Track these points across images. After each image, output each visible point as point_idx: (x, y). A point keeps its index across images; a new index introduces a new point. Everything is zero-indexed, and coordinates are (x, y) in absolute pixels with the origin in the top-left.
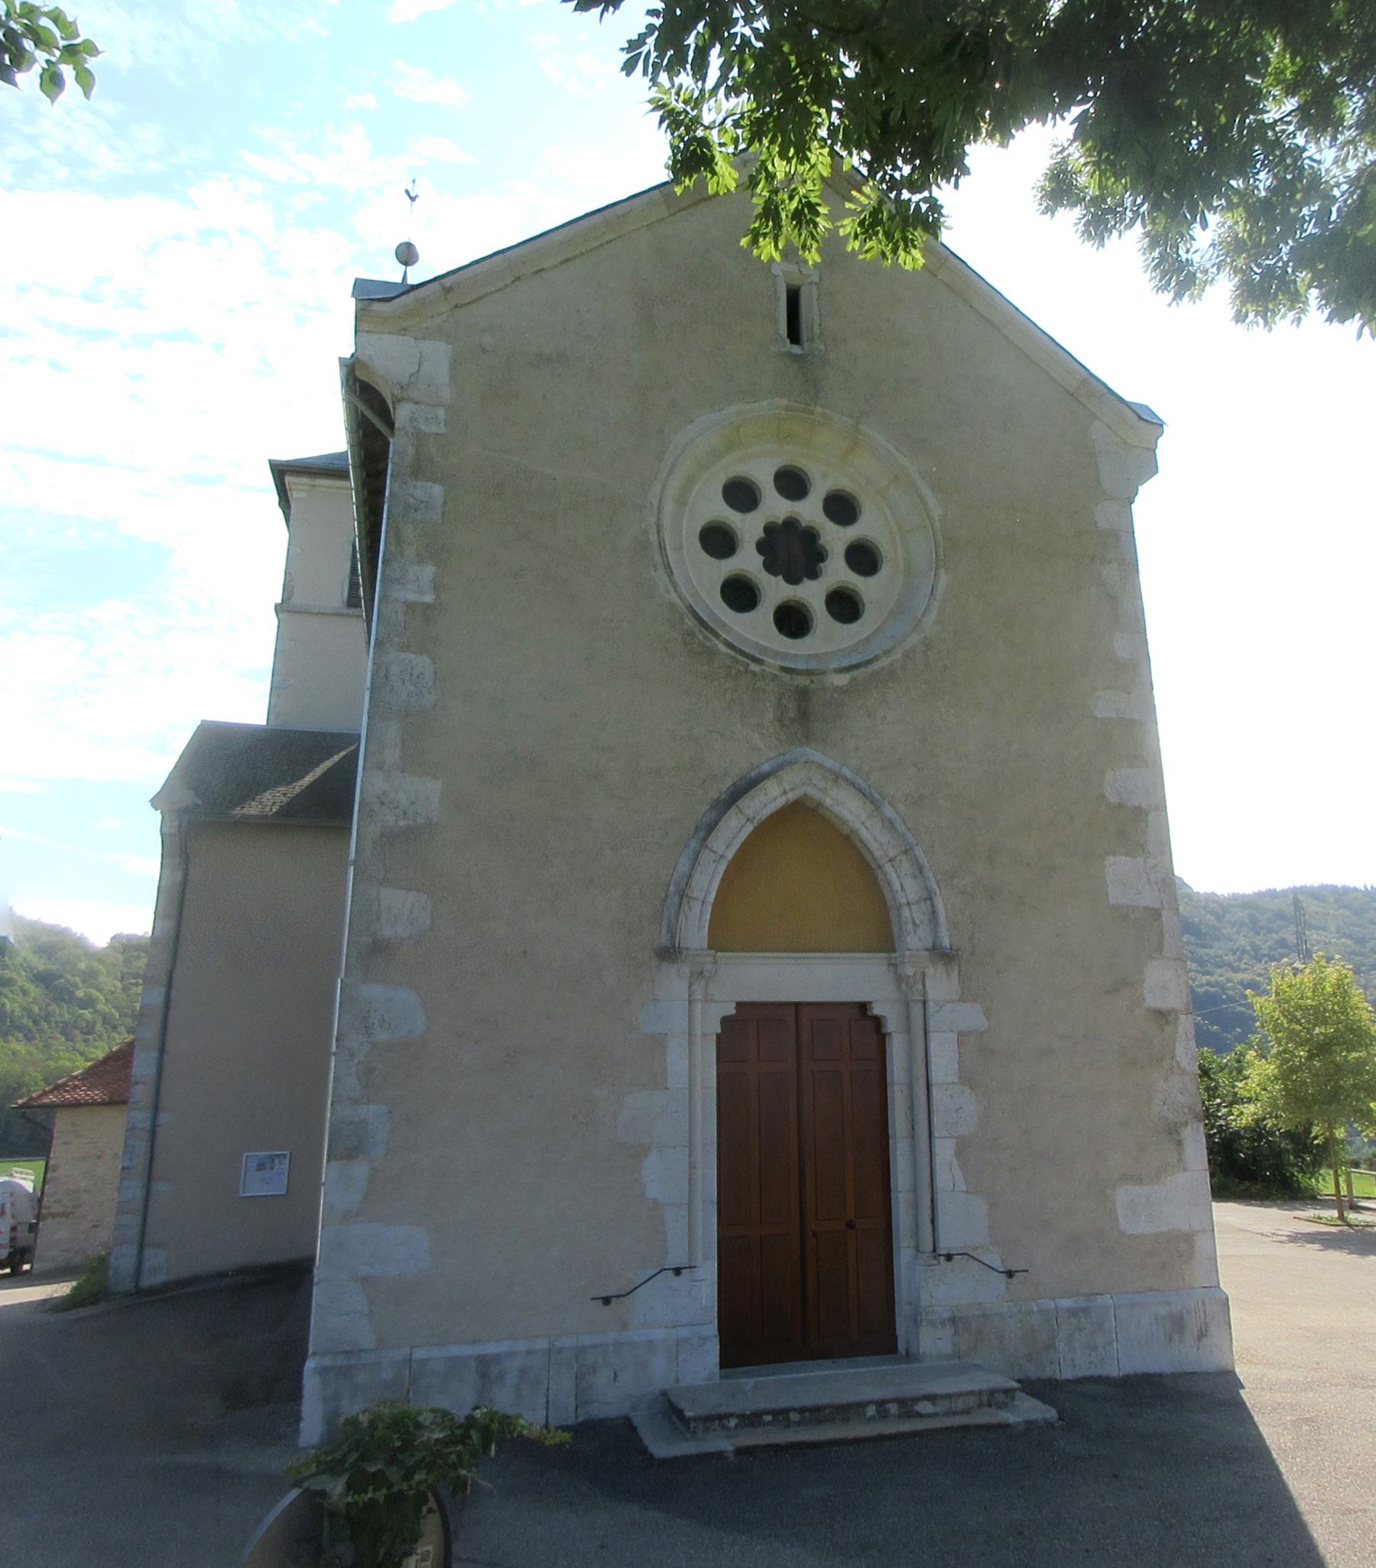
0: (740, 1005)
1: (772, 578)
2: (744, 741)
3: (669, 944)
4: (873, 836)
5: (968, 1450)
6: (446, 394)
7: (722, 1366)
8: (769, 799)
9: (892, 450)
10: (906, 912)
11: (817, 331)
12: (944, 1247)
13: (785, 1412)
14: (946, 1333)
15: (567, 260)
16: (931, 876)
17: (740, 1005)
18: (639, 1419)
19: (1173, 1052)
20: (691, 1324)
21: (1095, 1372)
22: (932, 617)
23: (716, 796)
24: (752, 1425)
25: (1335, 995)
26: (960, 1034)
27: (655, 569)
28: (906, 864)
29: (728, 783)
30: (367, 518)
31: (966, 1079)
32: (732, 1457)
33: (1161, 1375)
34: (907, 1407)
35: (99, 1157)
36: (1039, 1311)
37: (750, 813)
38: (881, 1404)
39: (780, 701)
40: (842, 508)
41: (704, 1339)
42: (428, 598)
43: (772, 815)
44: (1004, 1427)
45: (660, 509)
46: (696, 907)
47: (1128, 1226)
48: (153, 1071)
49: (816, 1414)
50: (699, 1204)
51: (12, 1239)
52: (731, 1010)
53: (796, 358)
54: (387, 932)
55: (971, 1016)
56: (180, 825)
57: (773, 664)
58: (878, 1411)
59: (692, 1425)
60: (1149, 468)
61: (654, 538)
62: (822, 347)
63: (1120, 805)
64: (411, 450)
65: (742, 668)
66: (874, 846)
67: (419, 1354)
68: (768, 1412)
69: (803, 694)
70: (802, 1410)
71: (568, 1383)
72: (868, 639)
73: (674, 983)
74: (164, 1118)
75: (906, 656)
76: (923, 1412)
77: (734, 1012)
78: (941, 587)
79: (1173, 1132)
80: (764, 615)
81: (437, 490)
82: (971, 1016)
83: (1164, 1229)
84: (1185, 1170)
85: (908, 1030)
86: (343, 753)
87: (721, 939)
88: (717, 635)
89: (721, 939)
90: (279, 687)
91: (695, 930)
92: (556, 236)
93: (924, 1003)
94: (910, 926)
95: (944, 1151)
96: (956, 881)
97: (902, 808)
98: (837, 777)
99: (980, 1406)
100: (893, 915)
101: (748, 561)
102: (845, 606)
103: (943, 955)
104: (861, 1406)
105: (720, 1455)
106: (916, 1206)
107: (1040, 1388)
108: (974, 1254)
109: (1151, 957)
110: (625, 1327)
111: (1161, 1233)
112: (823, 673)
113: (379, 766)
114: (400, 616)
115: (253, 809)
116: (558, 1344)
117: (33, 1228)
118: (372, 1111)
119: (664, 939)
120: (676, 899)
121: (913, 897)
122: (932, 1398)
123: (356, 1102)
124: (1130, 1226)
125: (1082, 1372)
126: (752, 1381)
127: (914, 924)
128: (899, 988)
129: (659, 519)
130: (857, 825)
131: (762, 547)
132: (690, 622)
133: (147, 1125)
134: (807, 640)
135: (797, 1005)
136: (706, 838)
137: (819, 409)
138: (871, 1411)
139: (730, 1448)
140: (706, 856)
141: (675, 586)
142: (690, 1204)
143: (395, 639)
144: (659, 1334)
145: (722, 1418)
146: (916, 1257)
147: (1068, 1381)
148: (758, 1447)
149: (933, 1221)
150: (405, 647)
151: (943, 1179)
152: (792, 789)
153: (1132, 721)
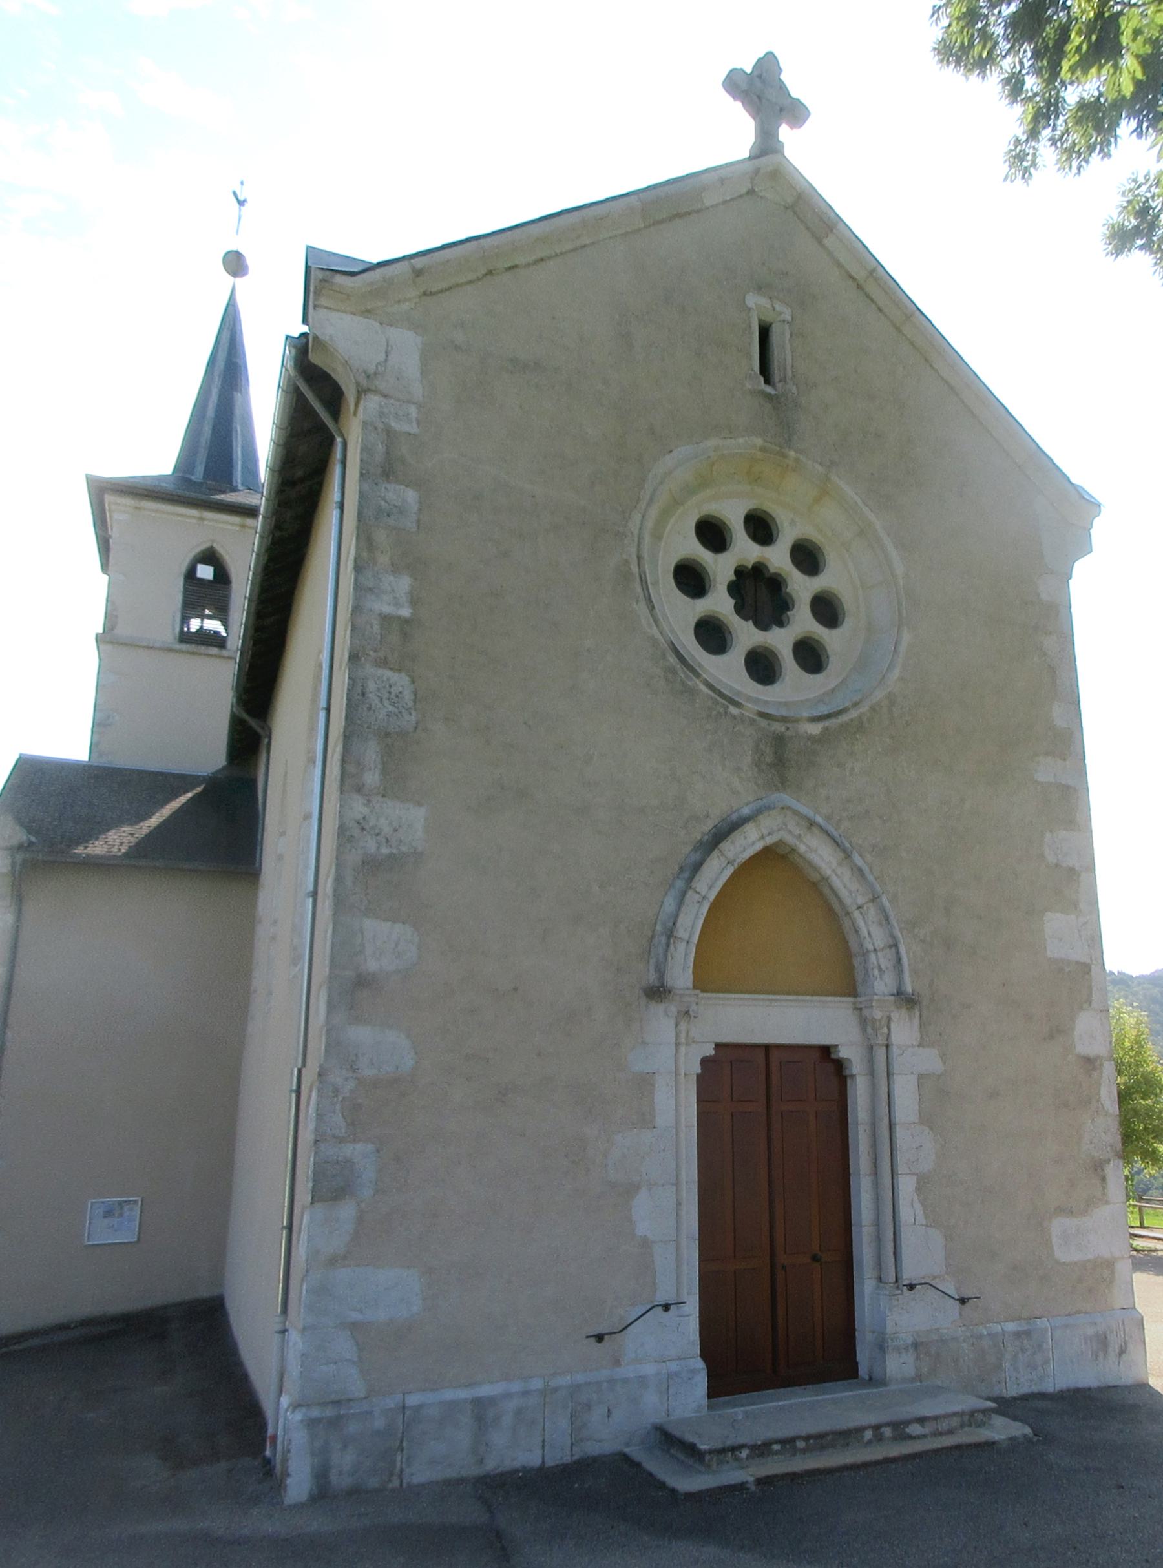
0: (718, 1046)
2: (725, 785)
3: (657, 984)
4: (844, 883)
5: (954, 1471)
6: (418, 390)
7: (710, 1396)
8: (746, 843)
10: (872, 957)
11: (789, 374)
12: (908, 1275)
14: (909, 1358)
16: (896, 925)
17: (718, 1046)
18: (636, 1452)
19: (1098, 1094)
22: (896, 673)
23: (699, 838)
24: (762, 1455)
25: (1132, 1049)
26: (920, 1077)
27: (637, 602)
28: (872, 912)
29: (708, 826)
30: (272, 532)
31: (926, 1119)
32: (753, 1488)
33: (1090, 1389)
34: (899, 1429)
36: (989, 1335)
37: (730, 855)
38: (877, 1428)
39: (757, 746)
40: (807, 557)
41: (693, 1372)
42: (406, 612)
43: (752, 858)
44: (990, 1445)
45: (640, 538)
46: (682, 947)
47: (1061, 1255)
49: (820, 1441)
50: (684, 1242)
52: (710, 1051)
53: (769, 397)
54: (372, 966)
55: (929, 1060)
56: (13, 864)
57: (750, 709)
58: (875, 1436)
59: (707, 1457)
60: (1084, 547)
61: (635, 569)
62: (794, 390)
63: (1057, 865)
64: (381, 448)
65: (722, 710)
67: (413, 1400)
68: (778, 1442)
69: (779, 741)
70: (807, 1438)
71: (564, 1423)
72: (833, 690)
73: (661, 1022)
75: (873, 709)
76: (914, 1434)
77: (713, 1052)
79: (1098, 1167)
80: (736, 658)
81: (411, 496)
82: (929, 1060)
83: (1090, 1256)
84: (1107, 1203)
85: (872, 1073)
86: (190, 795)
87: (703, 982)
88: (698, 675)
89: (703, 982)
90: (100, 725)
91: (681, 974)
92: (535, 230)
93: (887, 1046)
94: (876, 972)
95: (907, 1185)
96: (916, 930)
97: (869, 857)
98: (812, 824)
99: (962, 1426)
100: (856, 962)
101: (719, 603)
102: (810, 656)
103: (907, 1000)
104: (860, 1430)
105: (741, 1487)
106: (878, 1238)
107: (1006, 1406)
108: (933, 1283)
109: (1081, 1008)
110: (617, 1363)
111: (1089, 1261)
112: (797, 721)
113: (359, 789)
116: (553, 1383)
118: (357, 1151)
119: (652, 978)
120: (663, 939)
121: (880, 944)
122: (922, 1420)
123: (341, 1140)
124: (1065, 1254)
125: (1025, 1390)
126: (739, 1410)
127: (880, 969)
128: (864, 1030)
130: (829, 872)
131: (734, 589)
132: (672, 659)
135: (767, 1048)
136: (690, 879)
137: (792, 453)
138: (868, 1435)
141: (656, 622)
142: (677, 1242)
143: (371, 653)
144: (649, 1369)
145: (734, 1449)
146: (878, 1288)
147: (1014, 1399)
148: (776, 1476)
149: (895, 1254)
150: (383, 663)
151: (905, 1213)
152: (769, 834)
153: (1068, 787)
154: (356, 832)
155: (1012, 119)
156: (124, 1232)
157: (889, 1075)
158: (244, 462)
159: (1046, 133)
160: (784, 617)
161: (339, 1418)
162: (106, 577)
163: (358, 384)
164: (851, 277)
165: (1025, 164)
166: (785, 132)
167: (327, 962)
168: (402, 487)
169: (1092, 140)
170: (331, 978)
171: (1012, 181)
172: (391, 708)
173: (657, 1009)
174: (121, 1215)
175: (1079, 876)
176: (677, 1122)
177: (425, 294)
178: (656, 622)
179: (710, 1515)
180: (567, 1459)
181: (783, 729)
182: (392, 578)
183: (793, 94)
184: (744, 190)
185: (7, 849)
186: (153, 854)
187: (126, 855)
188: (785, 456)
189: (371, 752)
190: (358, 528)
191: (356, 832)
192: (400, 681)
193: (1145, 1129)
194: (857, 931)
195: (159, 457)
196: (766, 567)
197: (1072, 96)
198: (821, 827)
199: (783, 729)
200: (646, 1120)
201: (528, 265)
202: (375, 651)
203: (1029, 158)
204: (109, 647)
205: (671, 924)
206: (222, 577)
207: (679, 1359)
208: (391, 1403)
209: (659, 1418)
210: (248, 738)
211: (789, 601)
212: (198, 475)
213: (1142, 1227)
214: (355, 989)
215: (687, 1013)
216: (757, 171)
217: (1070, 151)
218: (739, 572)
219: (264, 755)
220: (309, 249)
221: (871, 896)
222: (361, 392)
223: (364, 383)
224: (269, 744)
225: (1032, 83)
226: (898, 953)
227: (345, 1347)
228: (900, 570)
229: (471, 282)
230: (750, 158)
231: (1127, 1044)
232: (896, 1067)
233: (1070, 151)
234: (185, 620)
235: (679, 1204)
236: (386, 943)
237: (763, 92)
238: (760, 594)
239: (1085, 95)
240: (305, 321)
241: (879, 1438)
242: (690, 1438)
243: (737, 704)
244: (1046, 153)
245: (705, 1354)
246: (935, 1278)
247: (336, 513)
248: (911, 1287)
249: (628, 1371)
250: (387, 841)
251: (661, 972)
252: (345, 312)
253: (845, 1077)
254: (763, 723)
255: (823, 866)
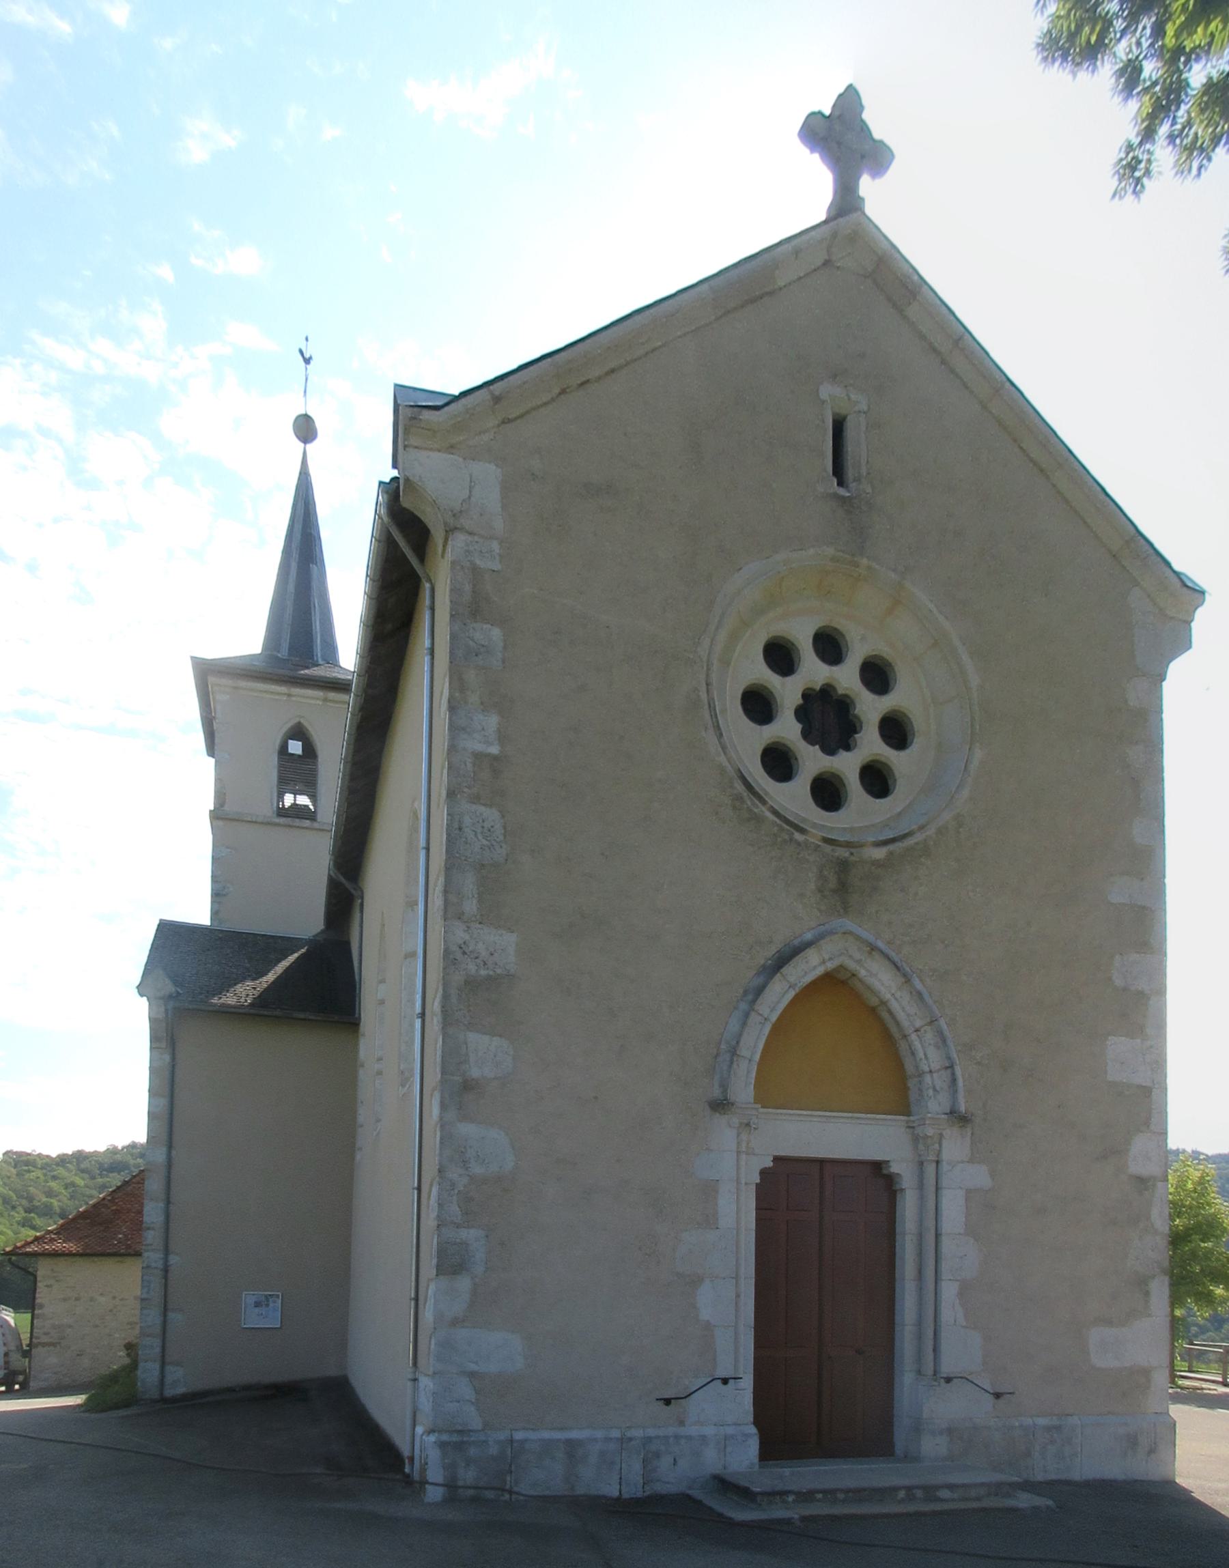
0: (777, 1159)
1: (811, 748)
2: (791, 910)
4: (903, 1009)
6: (499, 525)
9: (935, 610)
10: (928, 1079)
11: (864, 471)
12: (946, 1368)
13: (833, 1492)
15: (613, 371)
17: (777, 1159)
18: (697, 1494)
20: (735, 1424)
21: (1063, 1477)
23: (762, 962)
26: (968, 1191)
29: (773, 949)
30: (365, 691)
34: (930, 1492)
35: (77, 1299)
36: (1021, 1426)
37: (792, 979)
38: (909, 1489)
41: (747, 1436)
42: (494, 750)
48: (162, 1218)
49: (858, 1495)
51: (6, 1363)
52: (769, 1163)
54: (475, 1073)
55: (979, 1176)
56: (166, 1010)
57: (814, 837)
59: (759, 1498)
60: (1180, 642)
61: (704, 696)
62: (869, 490)
63: (1125, 989)
64: (468, 588)
65: (786, 837)
66: (901, 1016)
67: (519, 1436)
69: (843, 867)
70: (848, 1491)
71: (637, 1466)
72: (899, 814)
73: (724, 1132)
74: (173, 1259)
75: (940, 832)
77: (771, 1164)
78: (975, 763)
79: (1141, 1284)
81: (496, 633)
82: (979, 1176)
84: (1150, 1315)
85: (921, 1186)
86: (296, 955)
87: (766, 1096)
88: (764, 802)
89: (766, 1096)
90: (218, 895)
91: (743, 1090)
93: (937, 1162)
94: (931, 1092)
95: (949, 1291)
98: (873, 948)
100: (911, 1083)
101: (786, 728)
102: (877, 780)
103: (960, 1119)
104: (895, 1489)
105: (788, 1521)
106: (919, 1337)
110: (682, 1423)
112: (861, 846)
113: (460, 917)
114: (470, 766)
115: (229, 999)
116: (629, 1434)
117: (26, 1354)
118: (470, 1235)
119: (716, 1093)
120: (727, 1057)
121: (935, 1065)
122: (951, 1487)
124: (1099, 1360)
125: (1052, 1476)
126: (787, 1471)
127: (935, 1090)
129: (708, 675)
130: (888, 996)
131: (801, 713)
132: (739, 787)
133: (160, 1264)
134: (842, 813)
135: (821, 1162)
136: (754, 1001)
137: (865, 561)
138: (902, 1494)
139: (796, 1516)
140: (754, 1018)
141: (724, 748)
144: (709, 1431)
150: (475, 799)
151: (946, 1315)
152: (831, 959)
153: (1144, 908)
154: (459, 956)
155: (1124, 118)
156: (271, 1319)
157: (937, 1189)
158: (322, 635)
159: (1164, 130)
160: (851, 742)
161: (463, 1442)
162: (212, 761)
163: (446, 524)
164: (935, 350)
165: (1137, 174)
166: (867, 186)
167: (438, 1069)
168: (489, 626)
169: (1219, 129)
170: (443, 1082)
171: (1121, 198)
172: (485, 842)
173: (721, 1120)
174: (267, 1305)
175: (1149, 999)
176: (738, 1222)
177: (503, 422)
178: (724, 748)
179: (763, 1536)
180: (640, 1494)
181: (847, 854)
182: (481, 717)
183: (877, 135)
184: (819, 262)
185: (161, 998)
186: (269, 1008)
187: (251, 1005)
188: (857, 565)
189: (469, 883)
190: (450, 669)
191: (459, 956)
192: (491, 815)
193: (1202, 1270)
194: (913, 1054)
195: (245, 634)
196: (834, 689)
197: (1197, 76)
198: (882, 952)
199: (847, 854)
200: (710, 1221)
201: (599, 378)
202: (469, 787)
203: (1142, 165)
204: (221, 823)
205: (734, 1043)
206: (310, 751)
207: (735, 1424)
208: (502, 1436)
209: (717, 1469)
210: (343, 899)
211: (858, 725)
212: (284, 653)
213: (1190, 1371)
214: (461, 1091)
215: (748, 1125)
216: (835, 235)
217: (1190, 149)
218: (807, 695)
219: (357, 915)
220: (398, 387)
221: (928, 1020)
222: (450, 531)
223: (451, 521)
224: (362, 905)
225: (1151, 69)
226: (953, 1074)
227: (465, 1390)
228: (974, 680)
229: (545, 404)
230: (825, 222)
231: (1190, 1186)
232: (944, 1182)
233: (1190, 149)
234: (281, 797)
235: (738, 1296)
236: (487, 1052)
237: (842, 137)
238: (829, 718)
239: (1215, 74)
240: (395, 466)
241: (910, 1498)
242: (744, 1483)
243: (802, 831)
244: (1163, 155)
245: (757, 1422)
246: (971, 1374)
247: (427, 659)
248: (948, 1380)
249: (692, 1430)
250: (485, 964)
251: (724, 1087)
252: (431, 450)
253: (896, 1191)
254: (828, 848)
255: (883, 990)
